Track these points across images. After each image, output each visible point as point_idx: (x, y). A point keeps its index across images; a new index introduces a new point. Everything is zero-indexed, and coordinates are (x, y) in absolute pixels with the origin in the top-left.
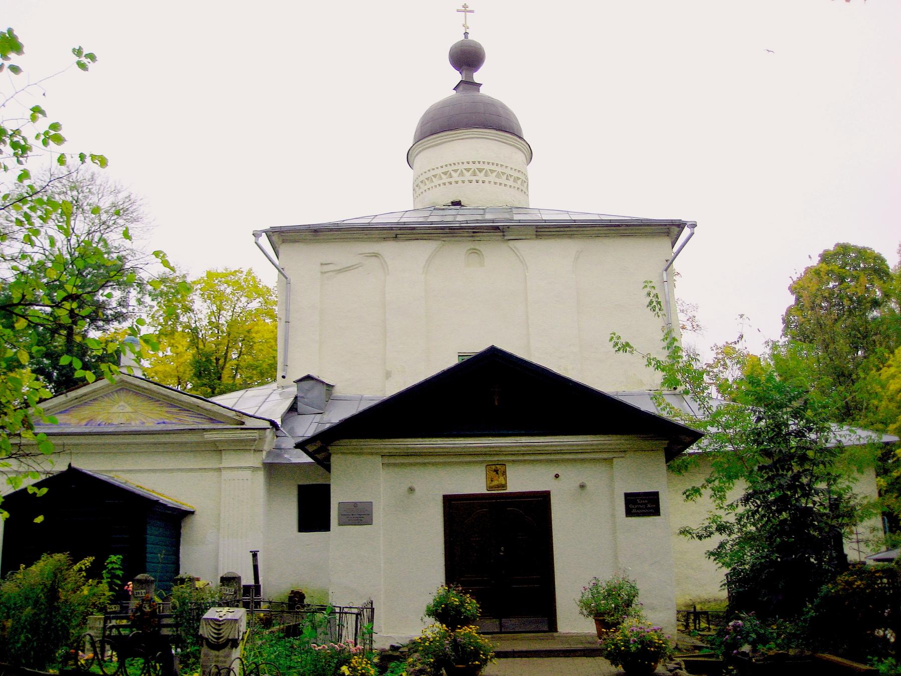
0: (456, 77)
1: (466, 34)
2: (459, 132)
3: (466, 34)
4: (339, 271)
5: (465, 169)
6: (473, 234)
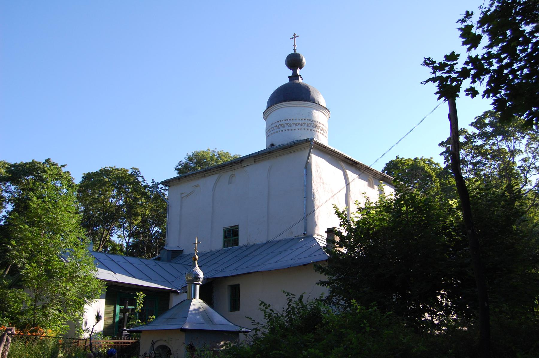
0: (290, 73)
1: (295, 50)
2: (273, 106)
3: (295, 50)
4: (187, 196)
5: (286, 124)
6: (231, 167)
